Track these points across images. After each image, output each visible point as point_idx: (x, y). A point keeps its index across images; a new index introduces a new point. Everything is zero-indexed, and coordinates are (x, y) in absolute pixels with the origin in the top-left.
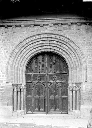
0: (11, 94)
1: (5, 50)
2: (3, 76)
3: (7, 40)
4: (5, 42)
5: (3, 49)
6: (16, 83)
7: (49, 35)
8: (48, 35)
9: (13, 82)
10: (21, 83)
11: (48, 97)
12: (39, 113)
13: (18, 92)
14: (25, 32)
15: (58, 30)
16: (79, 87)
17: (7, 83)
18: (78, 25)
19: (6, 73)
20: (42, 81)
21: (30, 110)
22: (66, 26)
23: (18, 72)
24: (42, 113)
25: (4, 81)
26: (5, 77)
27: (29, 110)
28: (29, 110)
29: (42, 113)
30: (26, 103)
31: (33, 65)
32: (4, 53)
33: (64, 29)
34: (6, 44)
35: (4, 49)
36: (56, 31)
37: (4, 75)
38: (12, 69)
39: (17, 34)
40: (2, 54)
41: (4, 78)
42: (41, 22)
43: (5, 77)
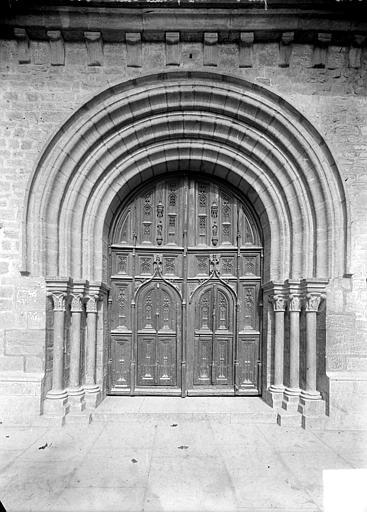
0: (40, 321)
1: (16, 138)
2: (6, 246)
3: (25, 96)
4: (18, 102)
5: (7, 134)
6: (64, 275)
7: (202, 83)
8: (197, 82)
9: (53, 275)
10: (87, 277)
11: (190, 335)
12: (211, 390)
13: (277, 314)
14: (104, 67)
15: (237, 64)
16: (318, 296)
17: (25, 273)
18: (170, 43)
19: (20, 234)
20: (169, 276)
21: (123, 380)
22: (272, 49)
23: (77, 234)
24: (152, 390)
25: (10, 268)
26: (17, 253)
27: (120, 380)
28: (120, 380)
29: (152, 390)
30: (109, 352)
31: (135, 212)
32: (12, 151)
33: (264, 61)
34: (23, 112)
35: (12, 132)
36: (232, 69)
37: (13, 242)
38: (46, 219)
39: (70, 74)
40: (5, 153)
41: (12, 256)
42: (170, 21)
43: (17, 253)
